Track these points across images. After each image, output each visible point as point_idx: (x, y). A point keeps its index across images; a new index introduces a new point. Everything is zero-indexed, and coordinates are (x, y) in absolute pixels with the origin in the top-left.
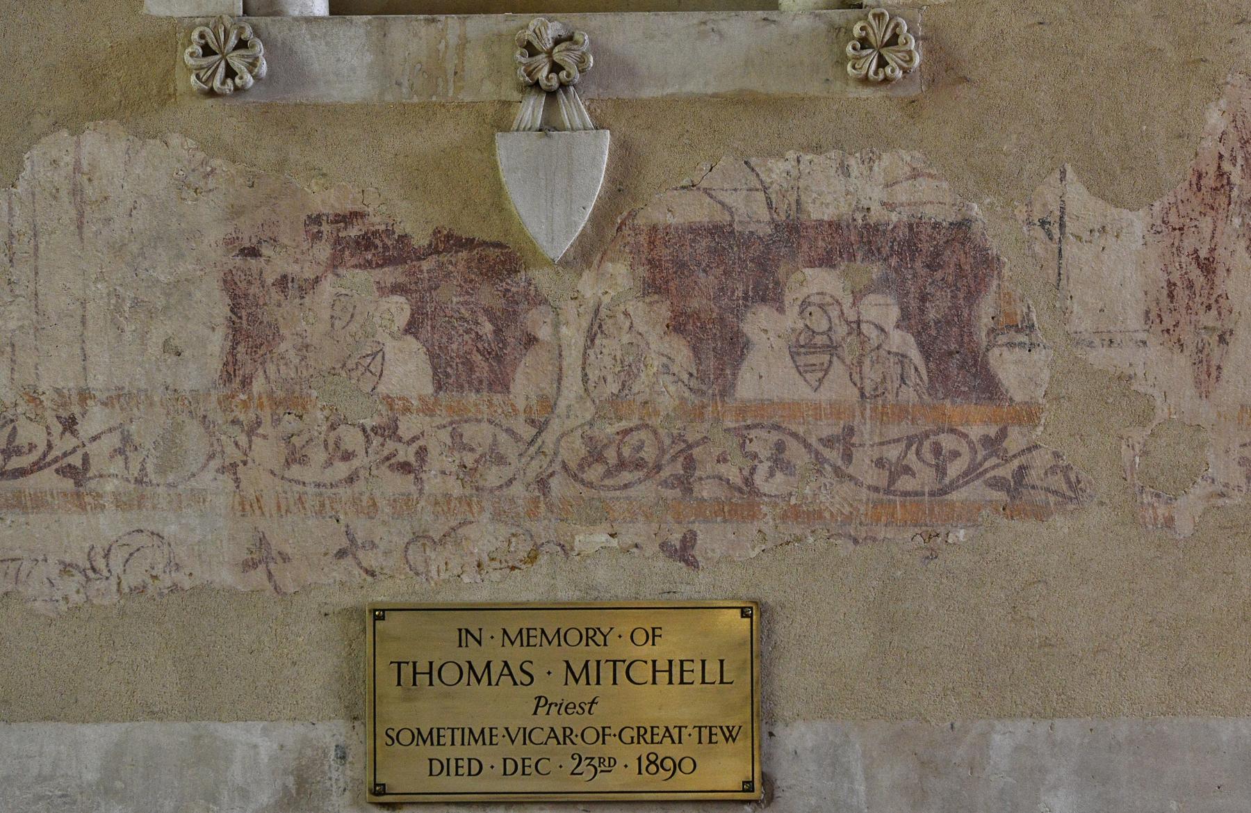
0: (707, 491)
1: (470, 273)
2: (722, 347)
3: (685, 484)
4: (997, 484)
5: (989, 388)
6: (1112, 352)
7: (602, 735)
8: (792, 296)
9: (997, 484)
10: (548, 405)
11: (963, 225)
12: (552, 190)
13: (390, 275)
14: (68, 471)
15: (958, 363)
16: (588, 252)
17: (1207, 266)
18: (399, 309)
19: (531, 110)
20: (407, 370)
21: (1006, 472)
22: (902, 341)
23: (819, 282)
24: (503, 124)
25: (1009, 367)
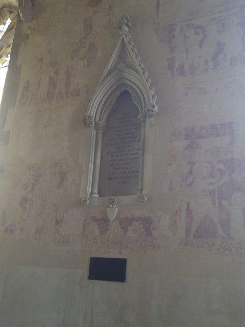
0: (123, 246)
1: (104, 222)
2: (125, 230)
3: (121, 245)
4: (152, 246)
5: (151, 235)
6: (138, 66)
7: (129, 172)
8: (133, 225)
9: (152, 246)
10: (109, 236)
11: (150, 217)
12: (113, 213)
13: (97, 223)
14: (68, 243)
15: (148, 232)
16: (115, 220)
17: (175, 222)
18: (97, 226)
19: (111, 206)
20: (97, 232)
21: (153, 245)
22: (143, 230)
23: (136, 223)
24: (108, 207)
25: (154, 233)
